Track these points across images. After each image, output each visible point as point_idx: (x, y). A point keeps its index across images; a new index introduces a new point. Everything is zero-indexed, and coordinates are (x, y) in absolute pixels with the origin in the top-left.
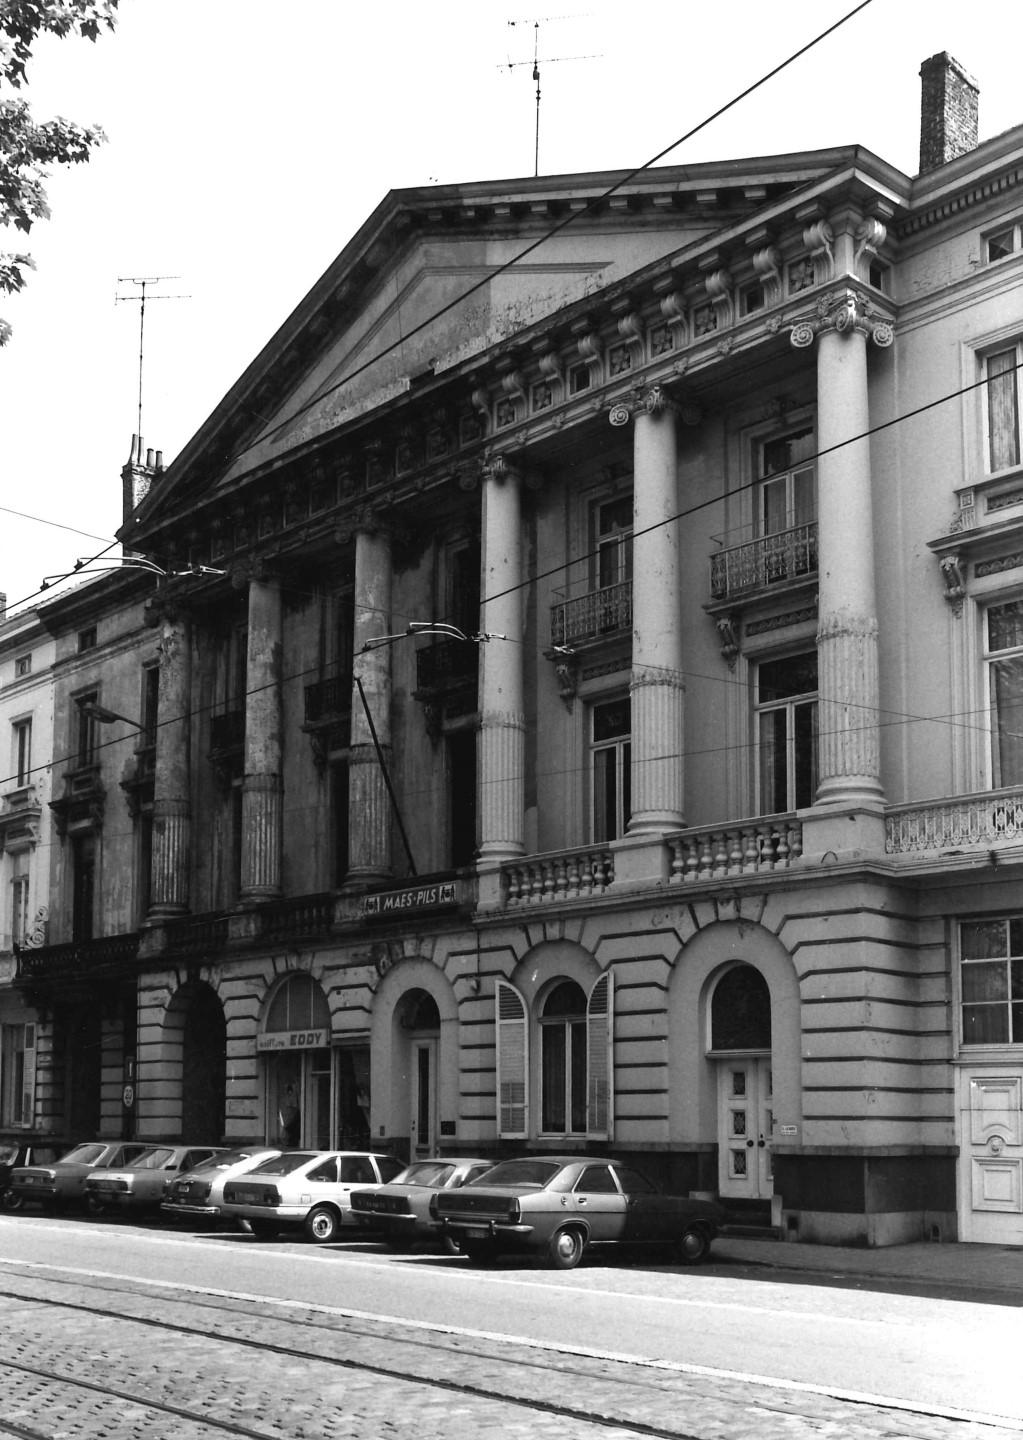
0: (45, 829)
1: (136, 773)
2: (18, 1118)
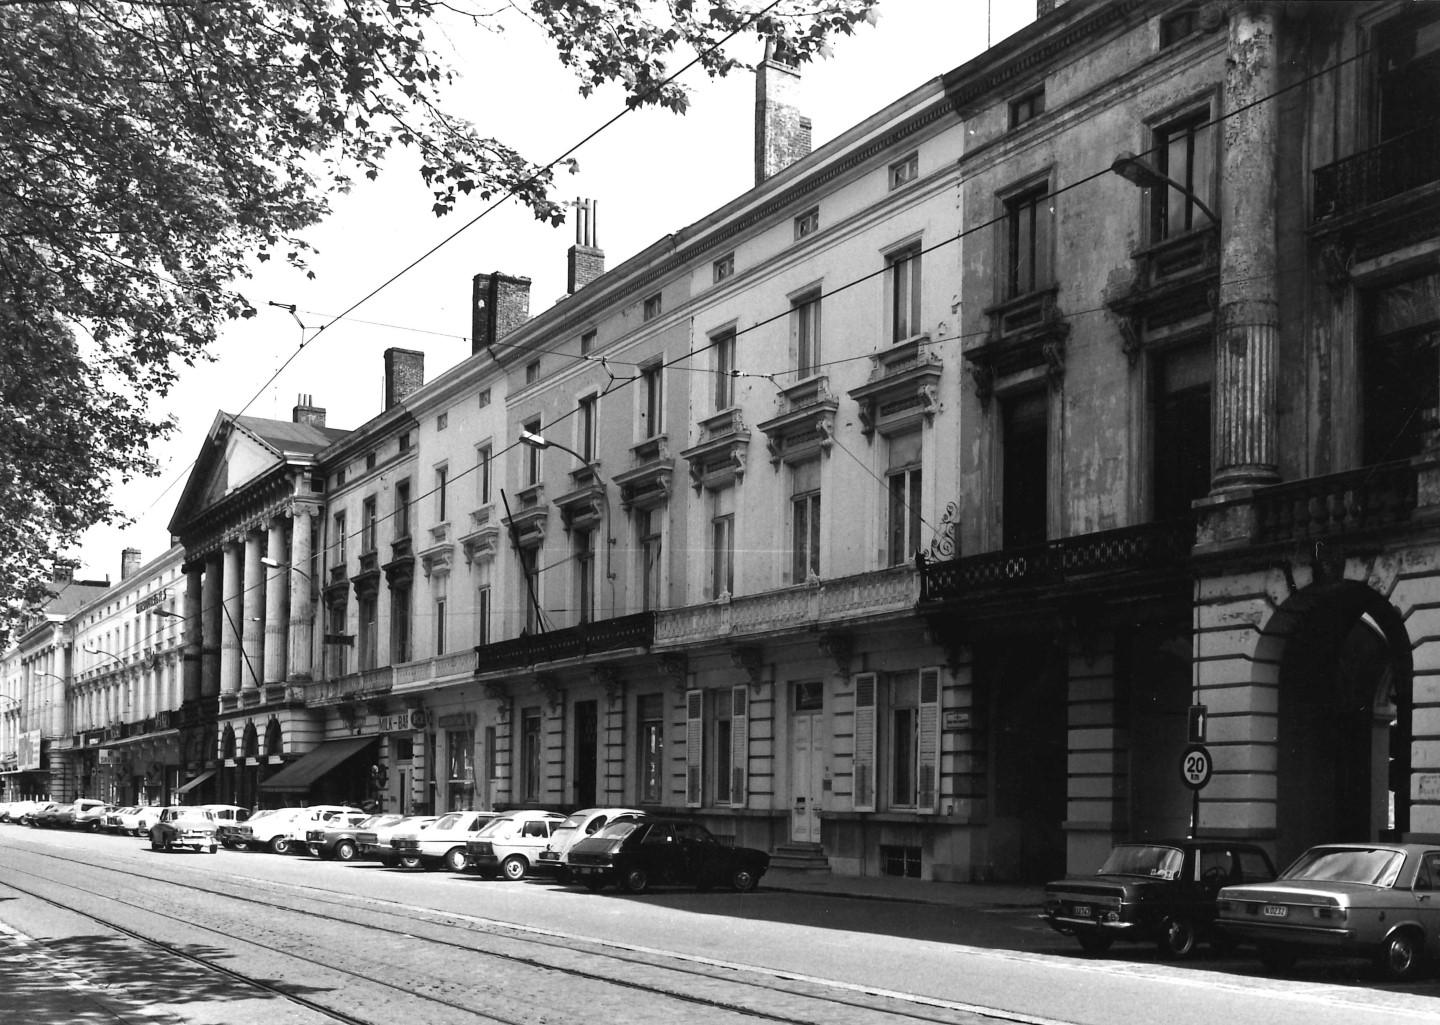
0: (951, 396)
1: (1134, 288)
2: (724, 794)
